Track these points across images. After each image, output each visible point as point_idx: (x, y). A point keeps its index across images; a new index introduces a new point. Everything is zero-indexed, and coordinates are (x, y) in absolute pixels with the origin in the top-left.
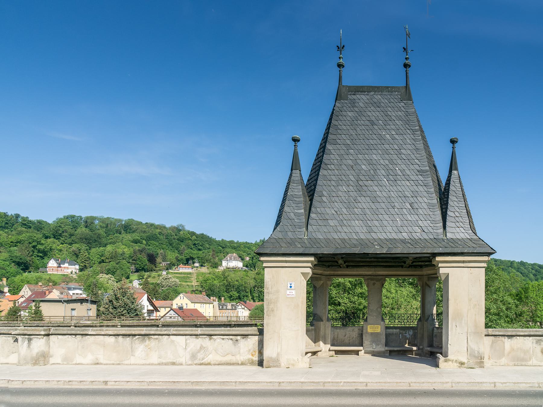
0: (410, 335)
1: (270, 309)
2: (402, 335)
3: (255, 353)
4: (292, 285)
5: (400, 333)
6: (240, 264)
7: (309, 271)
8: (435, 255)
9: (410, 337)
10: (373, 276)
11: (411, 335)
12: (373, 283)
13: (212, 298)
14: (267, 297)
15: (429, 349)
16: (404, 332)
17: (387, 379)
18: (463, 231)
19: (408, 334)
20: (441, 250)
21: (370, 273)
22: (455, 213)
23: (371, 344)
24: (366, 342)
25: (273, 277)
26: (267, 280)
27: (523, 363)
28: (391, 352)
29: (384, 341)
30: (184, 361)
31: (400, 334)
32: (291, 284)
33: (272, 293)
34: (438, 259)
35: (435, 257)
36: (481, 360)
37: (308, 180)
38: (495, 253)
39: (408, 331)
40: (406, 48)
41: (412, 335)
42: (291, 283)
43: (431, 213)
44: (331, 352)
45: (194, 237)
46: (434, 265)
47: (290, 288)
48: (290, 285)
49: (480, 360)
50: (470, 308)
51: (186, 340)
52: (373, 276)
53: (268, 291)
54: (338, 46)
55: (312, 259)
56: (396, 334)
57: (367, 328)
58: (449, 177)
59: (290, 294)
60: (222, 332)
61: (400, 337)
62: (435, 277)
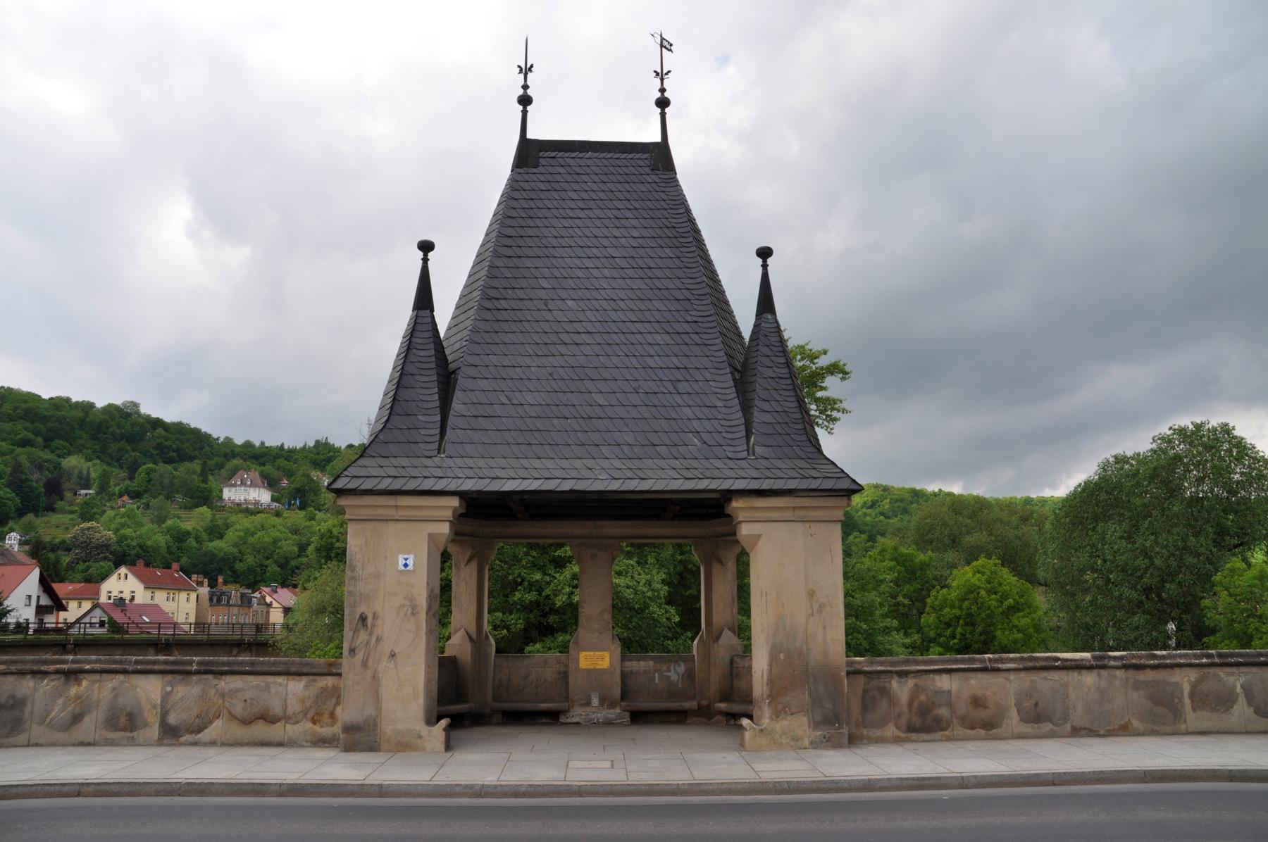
0: (679, 675)
4: (408, 562)
5: (656, 671)
6: (263, 496)
9: (678, 679)
11: (680, 676)
13: (194, 577)
14: (351, 589)
16: (665, 668)
17: (358, 643)
19: (673, 671)
20: (739, 485)
25: (366, 542)
26: (352, 548)
31: (654, 674)
32: (406, 559)
35: (730, 500)
37: (449, 329)
38: (861, 490)
39: (673, 665)
40: (659, 71)
41: (683, 675)
42: (406, 556)
43: (719, 404)
45: (160, 431)
46: (729, 516)
47: (403, 568)
48: (404, 562)
54: (519, 67)
55: (455, 502)
57: (577, 660)
58: (758, 325)
62: (730, 535)
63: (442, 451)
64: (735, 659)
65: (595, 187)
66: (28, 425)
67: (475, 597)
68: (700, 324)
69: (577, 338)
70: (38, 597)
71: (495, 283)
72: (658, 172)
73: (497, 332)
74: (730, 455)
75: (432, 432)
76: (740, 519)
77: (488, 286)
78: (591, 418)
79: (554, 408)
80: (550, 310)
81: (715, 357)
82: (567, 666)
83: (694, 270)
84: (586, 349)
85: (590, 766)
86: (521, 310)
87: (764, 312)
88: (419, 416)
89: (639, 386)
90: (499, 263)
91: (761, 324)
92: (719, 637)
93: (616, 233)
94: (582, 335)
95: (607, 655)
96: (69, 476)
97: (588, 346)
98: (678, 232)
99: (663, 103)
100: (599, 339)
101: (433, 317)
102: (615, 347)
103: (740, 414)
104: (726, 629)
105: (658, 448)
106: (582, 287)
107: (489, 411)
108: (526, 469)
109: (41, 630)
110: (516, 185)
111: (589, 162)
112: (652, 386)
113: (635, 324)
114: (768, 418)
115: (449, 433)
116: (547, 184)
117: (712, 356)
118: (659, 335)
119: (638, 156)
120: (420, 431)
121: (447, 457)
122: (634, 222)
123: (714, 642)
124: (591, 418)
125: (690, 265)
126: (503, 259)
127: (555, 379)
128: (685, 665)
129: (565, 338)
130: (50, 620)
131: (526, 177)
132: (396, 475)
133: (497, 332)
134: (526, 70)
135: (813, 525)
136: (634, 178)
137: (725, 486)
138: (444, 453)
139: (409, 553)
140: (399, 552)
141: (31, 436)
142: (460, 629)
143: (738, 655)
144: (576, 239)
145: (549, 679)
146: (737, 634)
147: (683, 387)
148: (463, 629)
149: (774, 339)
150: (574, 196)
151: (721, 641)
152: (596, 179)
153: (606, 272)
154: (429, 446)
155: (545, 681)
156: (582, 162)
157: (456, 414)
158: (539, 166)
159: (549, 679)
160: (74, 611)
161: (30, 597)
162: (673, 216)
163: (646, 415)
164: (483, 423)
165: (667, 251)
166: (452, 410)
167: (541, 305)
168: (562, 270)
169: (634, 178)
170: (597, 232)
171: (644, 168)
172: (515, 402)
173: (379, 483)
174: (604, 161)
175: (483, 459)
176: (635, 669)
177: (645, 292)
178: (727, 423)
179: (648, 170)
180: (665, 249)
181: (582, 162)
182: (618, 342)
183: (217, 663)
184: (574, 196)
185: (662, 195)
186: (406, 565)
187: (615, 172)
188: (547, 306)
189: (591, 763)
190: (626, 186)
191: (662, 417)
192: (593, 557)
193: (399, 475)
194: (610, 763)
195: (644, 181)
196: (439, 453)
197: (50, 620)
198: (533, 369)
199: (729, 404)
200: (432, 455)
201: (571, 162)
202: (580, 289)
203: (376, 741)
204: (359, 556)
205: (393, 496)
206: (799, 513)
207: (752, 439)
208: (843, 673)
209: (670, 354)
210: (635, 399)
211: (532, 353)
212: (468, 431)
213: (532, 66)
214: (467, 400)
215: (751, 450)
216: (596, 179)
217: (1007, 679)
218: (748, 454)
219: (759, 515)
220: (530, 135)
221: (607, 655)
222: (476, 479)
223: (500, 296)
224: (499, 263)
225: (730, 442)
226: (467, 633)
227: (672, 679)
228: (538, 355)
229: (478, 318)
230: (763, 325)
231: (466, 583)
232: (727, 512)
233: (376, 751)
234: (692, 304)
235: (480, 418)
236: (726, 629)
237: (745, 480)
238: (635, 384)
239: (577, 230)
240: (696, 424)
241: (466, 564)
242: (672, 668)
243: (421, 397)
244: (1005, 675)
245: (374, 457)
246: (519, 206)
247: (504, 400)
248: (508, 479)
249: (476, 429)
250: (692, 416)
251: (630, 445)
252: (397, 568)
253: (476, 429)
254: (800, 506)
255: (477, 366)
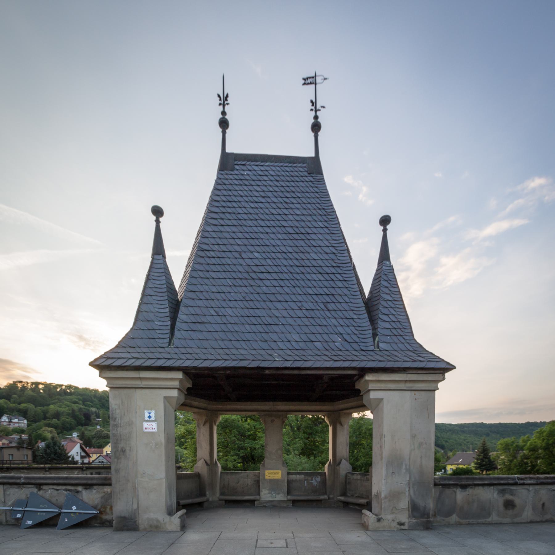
1: (120, 449)
2: (308, 482)
3: (104, 509)
4: (151, 415)
5: (305, 480)
7: (175, 393)
8: (363, 371)
9: (317, 484)
10: (272, 411)
12: (272, 420)
14: (114, 432)
15: (342, 498)
16: (310, 478)
18: (403, 341)
21: (267, 408)
22: (390, 316)
23: (269, 493)
24: (263, 490)
25: (122, 402)
27: (481, 521)
28: (294, 502)
29: (286, 489)
30: (5, 519)
31: (304, 482)
32: (150, 413)
33: (122, 426)
34: (368, 377)
36: (428, 520)
39: (314, 477)
40: (314, 101)
42: (149, 411)
43: (355, 317)
44: (221, 502)
48: (148, 415)
49: (427, 519)
50: (414, 447)
51: (4, 491)
52: (272, 411)
53: (115, 423)
56: (300, 480)
57: (264, 474)
59: (149, 427)
60: (55, 481)
61: (305, 484)
63: (172, 344)
64: (348, 474)
65: (271, 183)
66: (76, 397)
67: (209, 442)
68: (341, 268)
69: (261, 276)
70: (81, 453)
71: (206, 241)
72: (313, 175)
73: (208, 271)
74: (363, 348)
75: (165, 332)
76: (369, 388)
77: (201, 243)
78: (271, 325)
79: (246, 318)
80: (243, 258)
81: (352, 288)
82: (259, 477)
83: (337, 235)
84: (268, 283)
85: (272, 545)
86: (224, 258)
87: (384, 260)
88: (155, 322)
89: (302, 305)
90: (209, 228)
91: (382, 267)
92: (339, 463)
93: (286, 212)
94: (264, 274)
95: (280, 472)
96: (93, 414)
97: (268, 281)
98: (326, 212)
99: (316, 127)
100: (275, 276)
101: (165, 262)
102: (285, 281)
103: (369, 323)
104: (343, 459)
105: (315, 344)
106: (264, 244)
107: (204, 319)
108: (228, 354)
109: (83, 463)
110: (220, 181)
111: (268, 168)
112: (311, 306)
113: (299, 268)
114: (387, 325)
115: (176, 333)
116: (239, 181)
117: (350, 288)
118: (314, 275)
119: (299, 165)
120: (156, 331)
121: (175, 347)
122: (298, 206)
123: (337, 466)
124: (271, 325)
125: (335, 232)
126: (212, 226)
127: (247, 301)
128: (320, 477)
129: (253, 275)
130: (86, 460)
131: (226, 177)
132: (138, 357)
133: (208, 271)
134: (224, 100)
135: (416, 392)
136: (297, 179)
137: (362, 365)
138: (173, 345)
139: (151, 409)
140: (145, 409)
141: (77, 400)
142: (201, 459)
143: (349, 473)
144: (259, 215)
145: (249, 484)
146: (348, 461)
147: (331, 306)
148: (203, 459)
149: (391, 277)
150: (258, 189)
151: (341, 465)
152: (272, 178)
153: (279, 236)
154: (162, 341)
155: (248, 485)
156: (262, 168)
157: (181, 321)
158: (234, 170)
159: (249, 484)
160: (94, 457)
161: (78, 453)
162: (323, 202)
163: (307, 323)
164: (200, 327)
165: (320, 223)
166: (178, 318)
167: (237, 255)
168: (250, 234)
169: (297, 179)
170: (273, 211)
171: (304, 173)
172: (221, 314)
173: (126, 361)
174: (277, 168)
175: (199, 349)
176: (294, 479)
177: (305, 248)
178: (360, 329)
179: (306, 174)
180: (318, 222)
181: (262, 168)
182: (288, 278)
183: (71, 478)
184: (258, 189)
185: (316, 189)
186: (150, 417)
187: (285, 175)
188: (241, 256)
189: (272, 541)
190: (292, 184)
191: (317, 325)
192: (272, 421)
193: (140, 357)
194: (284, 541)
195: (303, 180)
196: (169, 345)
197: (86, 460)
198: (232, 294)
199: (361, 317)
200: (165, 346)
201: (256, 168)
202: (263, 245)
203: (136, 525)
204: (118, 411)
205: (138, 371)
206: (409, 385)
207: (377, 338)
208: (432, 486)
209: (323, 286)
210: (299, 313)
211: (231, 284)
212: (189, 332)
213: (227, 96)
214: (188, 313)
215: (376, 345)
216: (272, 178)
217: (528, 490)
218: (375, 348)
219: (383, 386)
220: (228, 150)
221: (280, 472)
222: (193, 360)
223: (210, 249)
224: (209, 228)
225: (363, 340)
226: (205, 460)
227: (314, 484)
228: (235, 286)
229: (195, 262)
230: (384, 268)
231: (204, 435)
232: (357, 387)
233: (137, 531)
234: (336, 256)
235: (196, 324)
236: (343, 459)
237: (375, 362)
238: (299, 304)
239: (260, 210)
240: (340, 329)
241: (203, 425)
242: (314, 479)
243: (157, 310)
244: (527, 487)
245: (125, 347)
246: (222, 194)
247: (214, 313)
248: (216, 360)
249: (194, 331)
250: (337, 324)
251: (297, 341)
252: (144, 419)
253: (194, 331)
254: (411, 379)
255: (194, 292)
